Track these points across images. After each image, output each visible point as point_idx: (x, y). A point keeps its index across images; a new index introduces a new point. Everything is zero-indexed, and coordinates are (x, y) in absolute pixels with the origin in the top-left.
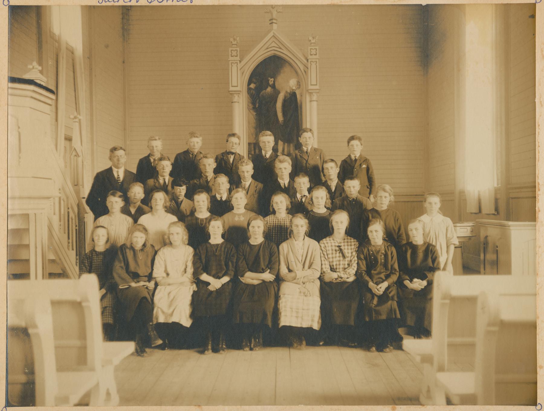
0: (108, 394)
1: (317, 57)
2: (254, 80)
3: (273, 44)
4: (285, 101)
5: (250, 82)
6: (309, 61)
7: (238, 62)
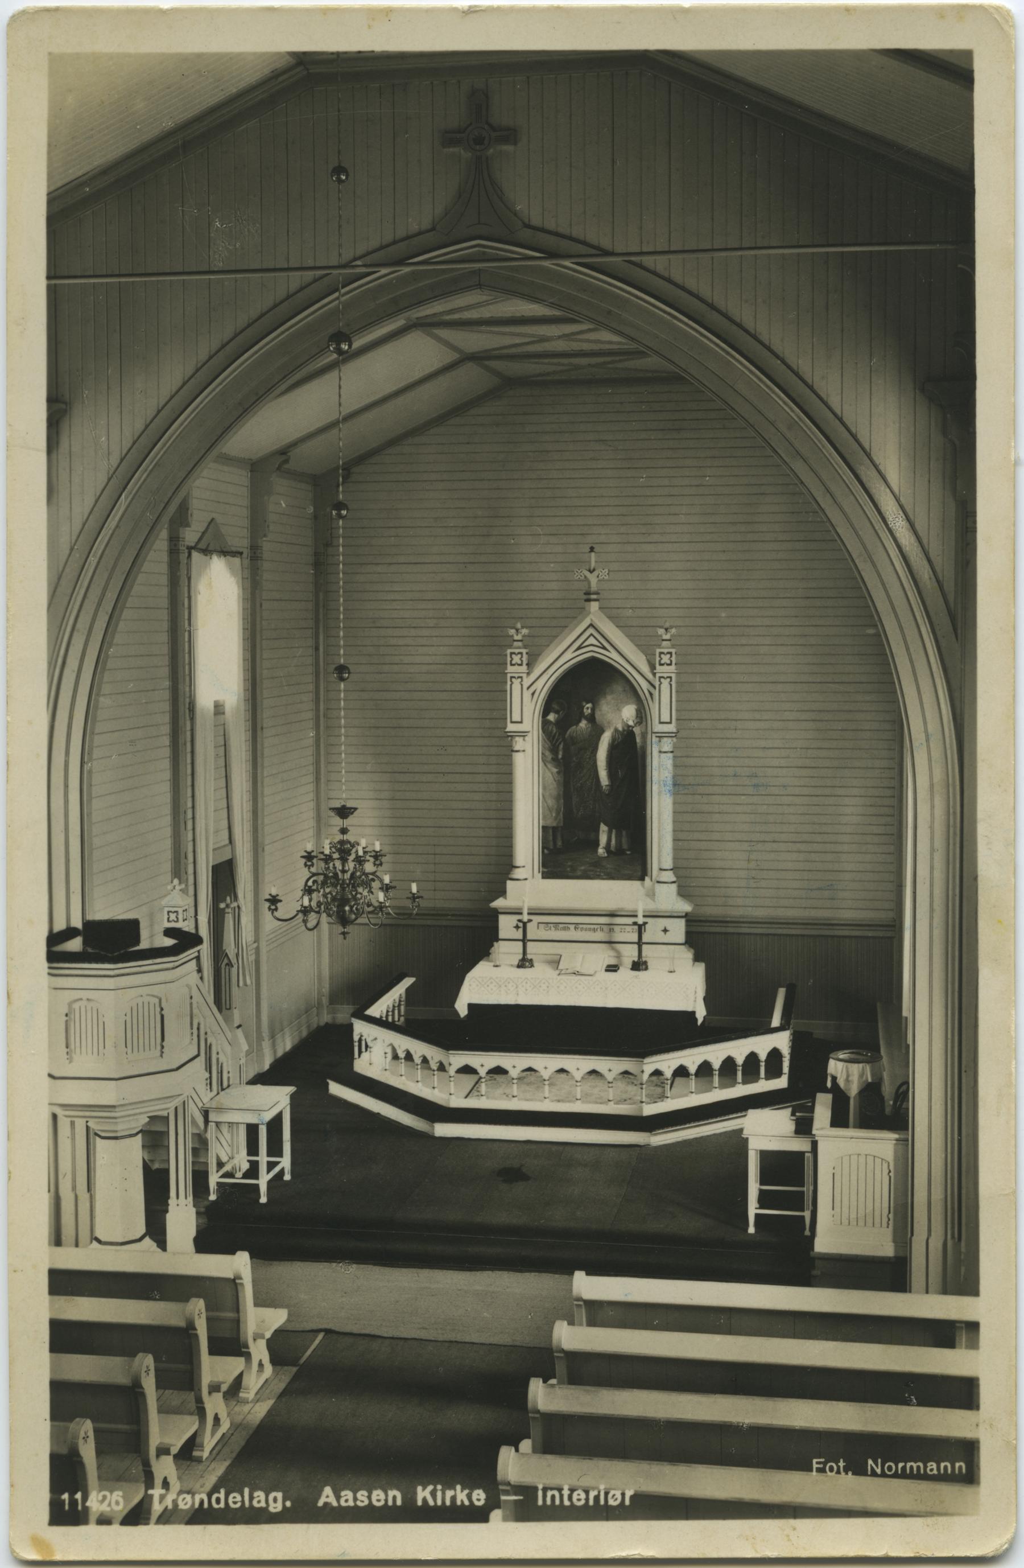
0: (261, 1365)
1: (673, 668)
2: (556, 706)
3: (592, 641)
4: (613, 748)
5: (546, 711)
6: (658, 675)
7: (524, 676)
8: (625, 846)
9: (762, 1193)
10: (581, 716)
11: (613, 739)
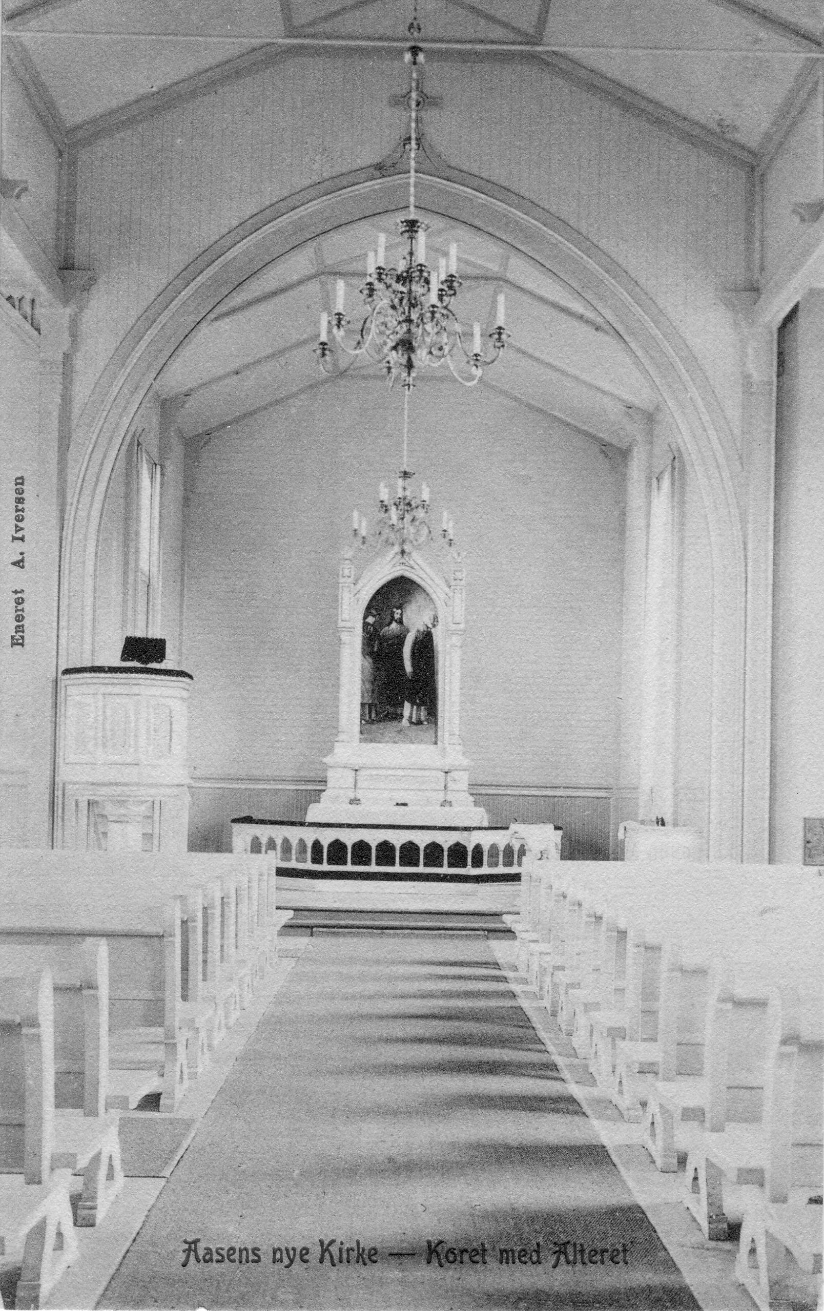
4: (415, 643)
8: (423, 719)
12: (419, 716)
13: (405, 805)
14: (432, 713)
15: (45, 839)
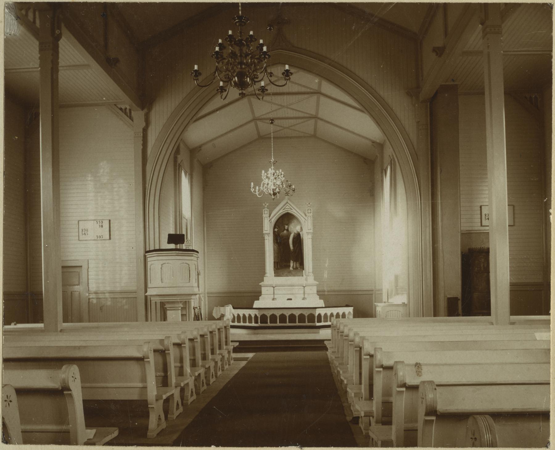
1: (311, 214)
3: (287, 207)
4: (294, 238)
8: (298, 267)
9: (324, 322)
10: (284, 229)
11: (294, 236)
12: (296, 266)
13: (288, 299)
14: (302, 264)
15: (144, 318)
